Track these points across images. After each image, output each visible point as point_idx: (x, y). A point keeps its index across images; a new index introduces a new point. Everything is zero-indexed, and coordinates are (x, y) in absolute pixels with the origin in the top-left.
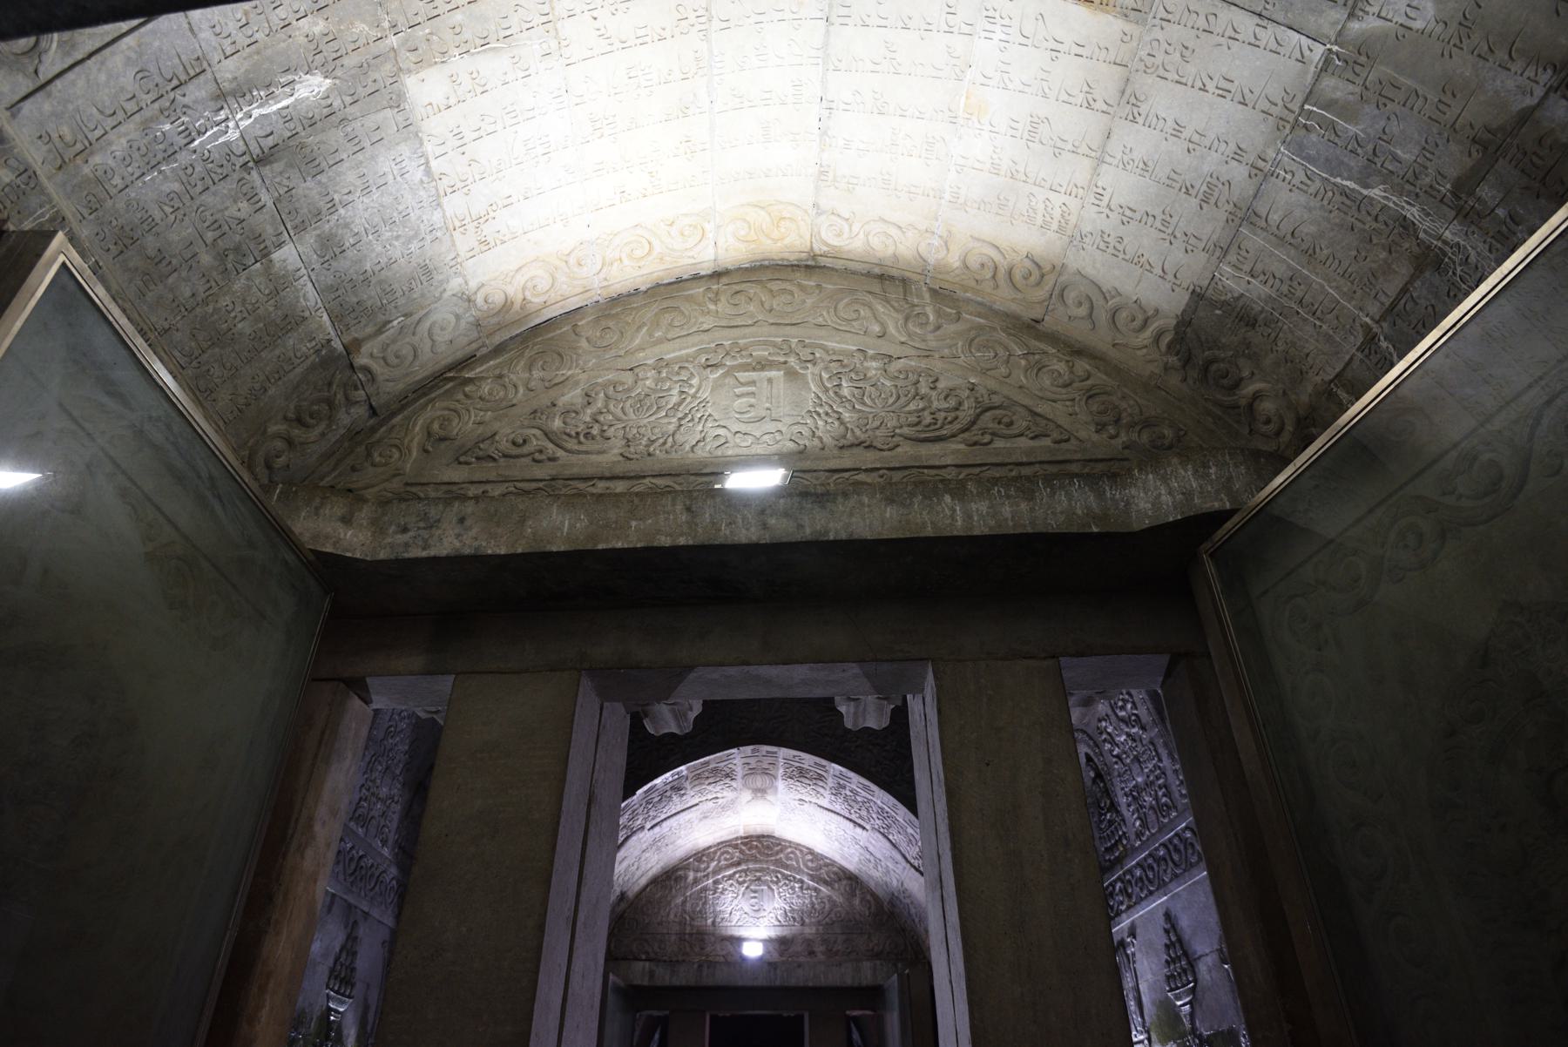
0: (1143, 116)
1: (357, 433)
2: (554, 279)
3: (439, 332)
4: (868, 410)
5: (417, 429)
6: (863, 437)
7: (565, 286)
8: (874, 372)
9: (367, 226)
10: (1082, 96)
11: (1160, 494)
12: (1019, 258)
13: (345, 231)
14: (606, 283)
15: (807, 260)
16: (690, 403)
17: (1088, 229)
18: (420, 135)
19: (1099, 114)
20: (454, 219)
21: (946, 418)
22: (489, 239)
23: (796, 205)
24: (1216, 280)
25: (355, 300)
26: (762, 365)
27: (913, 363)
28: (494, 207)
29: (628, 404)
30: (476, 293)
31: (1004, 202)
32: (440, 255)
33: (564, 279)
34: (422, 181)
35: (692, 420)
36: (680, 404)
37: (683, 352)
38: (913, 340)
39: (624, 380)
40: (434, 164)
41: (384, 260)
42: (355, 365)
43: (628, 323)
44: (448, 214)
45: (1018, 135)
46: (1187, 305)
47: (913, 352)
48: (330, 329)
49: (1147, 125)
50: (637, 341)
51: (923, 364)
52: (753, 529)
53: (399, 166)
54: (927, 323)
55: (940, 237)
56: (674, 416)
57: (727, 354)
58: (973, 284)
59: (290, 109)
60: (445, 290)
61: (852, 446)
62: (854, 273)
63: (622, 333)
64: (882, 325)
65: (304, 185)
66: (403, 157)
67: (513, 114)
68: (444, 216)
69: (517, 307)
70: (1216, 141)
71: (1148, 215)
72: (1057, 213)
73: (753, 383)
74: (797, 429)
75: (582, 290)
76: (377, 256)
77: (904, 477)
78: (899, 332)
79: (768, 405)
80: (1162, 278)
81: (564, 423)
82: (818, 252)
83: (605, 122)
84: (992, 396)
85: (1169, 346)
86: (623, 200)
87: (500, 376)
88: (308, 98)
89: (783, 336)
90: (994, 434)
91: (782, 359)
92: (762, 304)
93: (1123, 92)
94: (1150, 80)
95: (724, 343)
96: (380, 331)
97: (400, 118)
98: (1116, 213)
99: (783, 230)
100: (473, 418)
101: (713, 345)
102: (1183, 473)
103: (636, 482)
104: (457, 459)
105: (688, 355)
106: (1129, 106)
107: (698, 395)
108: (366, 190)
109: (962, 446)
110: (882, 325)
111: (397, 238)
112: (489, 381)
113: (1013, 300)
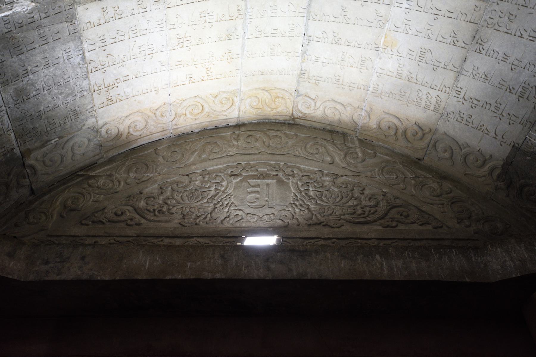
0: (485, 51)
1: (21, 204)
2: (147, 122)
3: (77, 148)
4: (324, 204)
5: (58, 203)
6: (322, 219)
7: (153, 127)
8: (328, 183)
9: (44, 85)
10: (450, 38)
11: (505, 260)
12: (411, 125)
13: (31, 87)
14: (175, 127)
15: (290, 120)
16: (221, 195)
17: (452, 110)
18: (82, 38)
19: (460, 49)
20: (95, 86)
21: (370, 211)
22: (113, 98)
23: (284, 90)
24: (527, 140)
25: (32, 127)
26: (263, 176)
27: (350, 179)
28: (118, 81)
29: (185, 195)
30: (101, 128)
31: (404, 94)
32: (84, 105)
33: (152, 123)
34: (79, 64)
35: (222, 205)
36: (215, 196)
37: (218, 167)
38: (350, 166)
39: (183, 181)
40: (87, 54)
41: (51, 106)
42: (26, 164)
43: (186, 149)
44: (91, 83)
45: (413, 58)
46: (509, 153)
47: (350, 173)
48: (15, 143)
49: (488, 55)
50: (192, 160)
51: (356, 180)
52: (261, 270)
53: (67, 54)
54: (357, 158)
55: (366, 111)
56: (212, 202)
57: (244, 169)
58: (383, 137)
59: (9, 17)
60: (84, 125)
61: (315, 224)
62: (315, 128)
63: (183, 155)
64: (332, 157)
65: (11, 59)
66: (71, 49)
67: (135, 32)
68: (89, 84)
69: (124, 137)
70: (528, 64)
71: (487, 103)
72: (434, 101)
73: (258, 186)
74: (283, 213)
75: (162, 130)
76: (48, 103)
77: (392, 243)
78: (342, 161)
79: (266, 199)
80: (495, 138)
81: (147, 204)
82: (296, 116)
83: (185, 39)
84: (396, 200)
85: (499, 176)
86: (191, 82)
87: (111, 175)
88: (20, 12)
89: (276, 161)
90: (398, 221)
91: (275, 173)
92: (264, 143)
93: (474, 37)
94: (490, 31)
95: (242, 163)
96: (43, 146)
97: (71, 28)
98: (468, 101)
99: (277, 103)
100: (92, 198)
101: (235, 164)
102: (518, 248)
103: (188, 240)
104: (81, 222)
105: (221, 169)
106: (478, 45)
107: (226, 191)
108: (47, 66)
109: (380, 228)
110: (332, 157)
111: (61, 93)
112: (104, 178)
113: (406, 147)
